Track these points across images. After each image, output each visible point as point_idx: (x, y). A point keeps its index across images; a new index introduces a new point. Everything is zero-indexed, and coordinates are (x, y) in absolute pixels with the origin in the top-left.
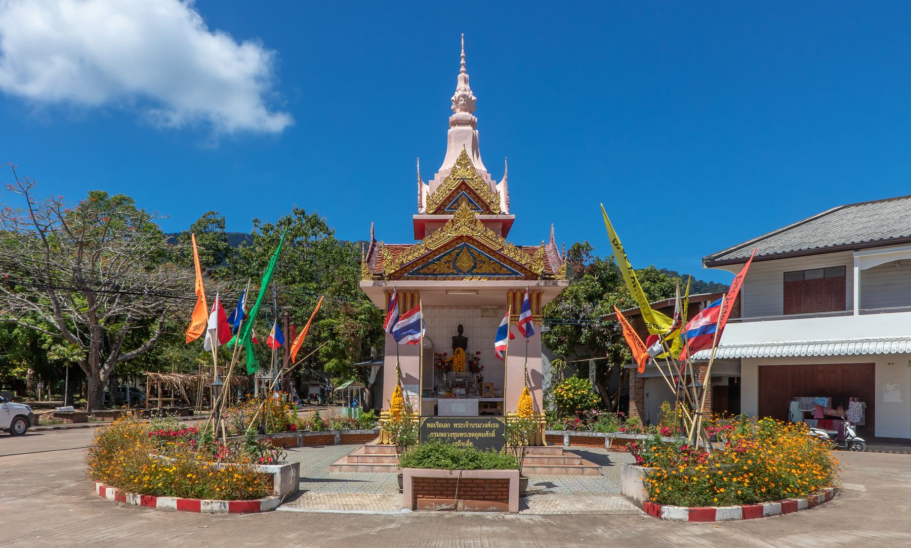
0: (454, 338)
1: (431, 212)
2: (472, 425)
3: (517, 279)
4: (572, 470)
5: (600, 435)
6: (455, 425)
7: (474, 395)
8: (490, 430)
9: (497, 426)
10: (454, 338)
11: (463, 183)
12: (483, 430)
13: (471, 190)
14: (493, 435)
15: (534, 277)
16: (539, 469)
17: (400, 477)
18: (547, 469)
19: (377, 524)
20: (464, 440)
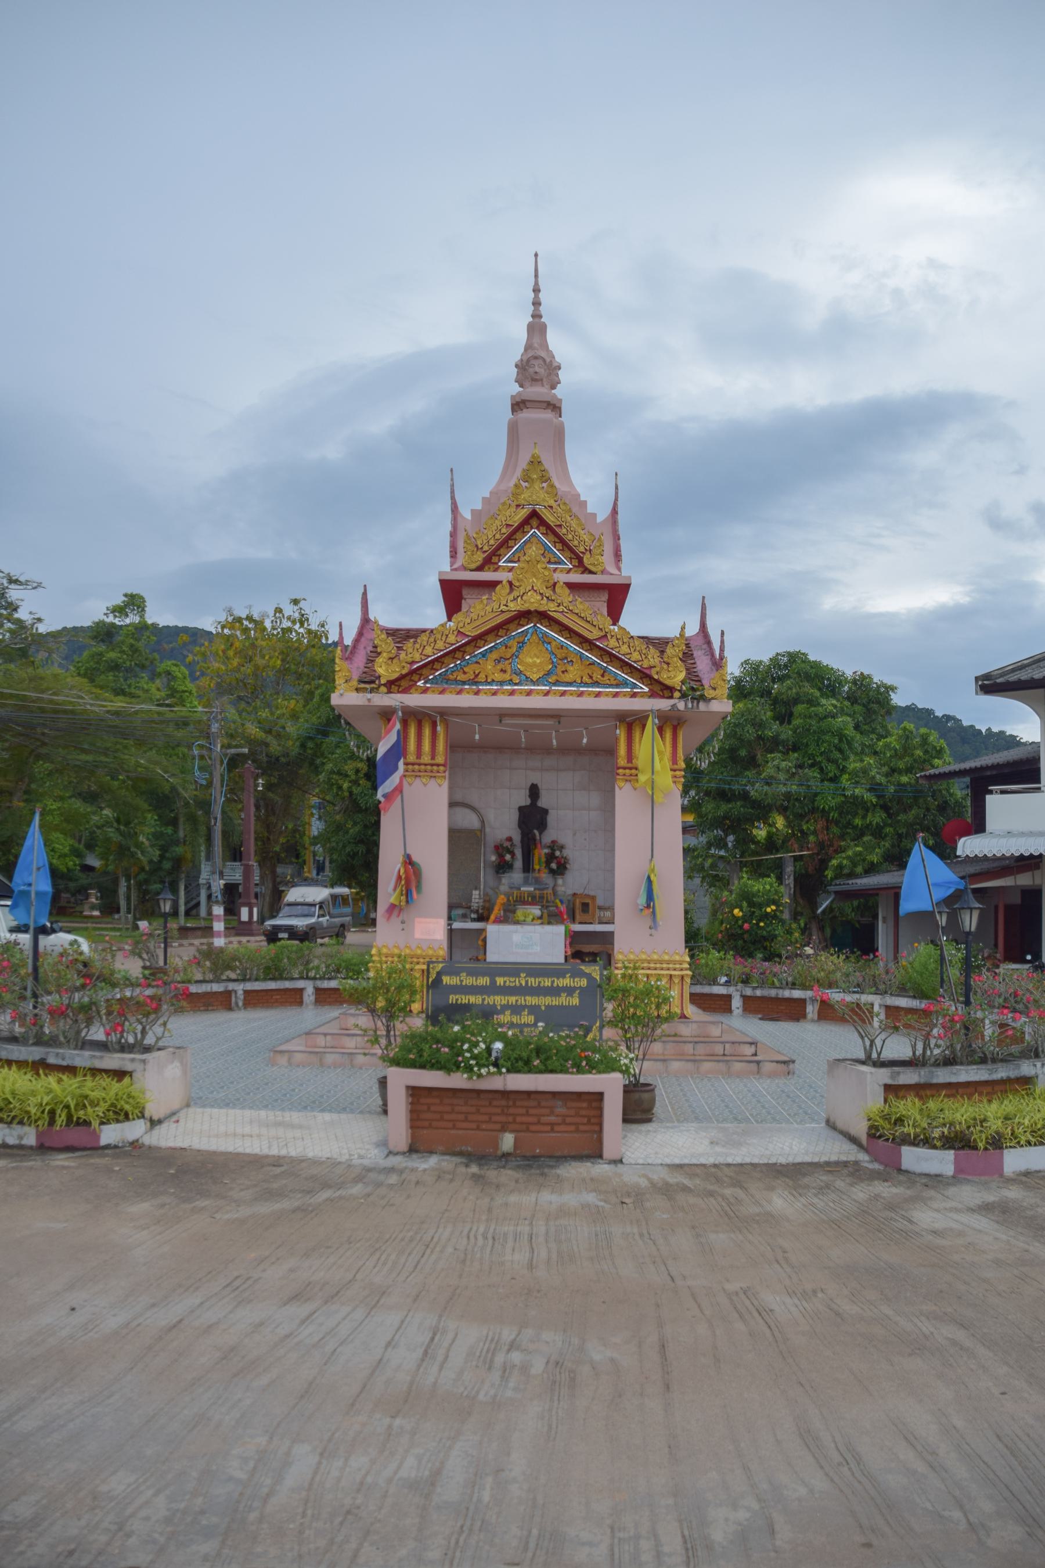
0: (521, 809)
1: (474, 566)
2: (533, 982)
3: (634, 695)
4: (738, 1066)
5: (797, 994)
6: (500, 981)
7: (561, 921)
8: (570, 991)
9: (584, 982)
10: (521, 809)
11: (534, 514)
12: (554, 991)
13: (548, 527)
14: (575, 1001)
15: (667, 693)
16: (675, 1065)
17: (383, 1082)
18: (690, 1065)
19: (326, 1185)
20: (516, 1010)
